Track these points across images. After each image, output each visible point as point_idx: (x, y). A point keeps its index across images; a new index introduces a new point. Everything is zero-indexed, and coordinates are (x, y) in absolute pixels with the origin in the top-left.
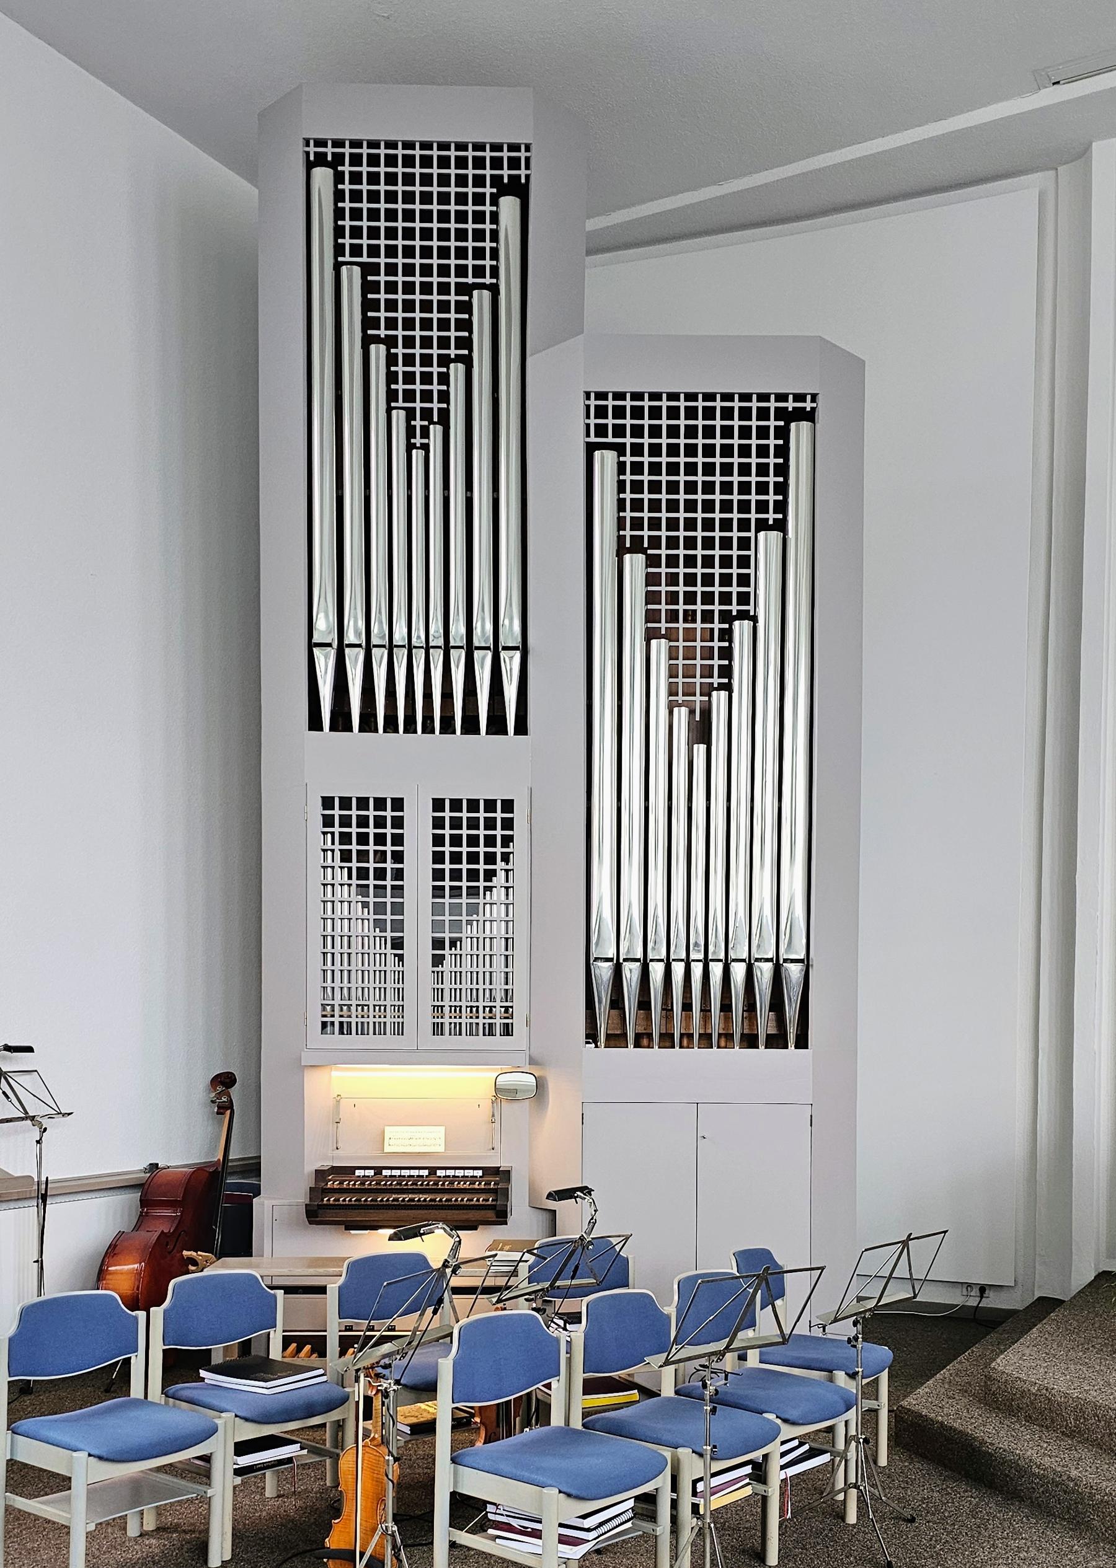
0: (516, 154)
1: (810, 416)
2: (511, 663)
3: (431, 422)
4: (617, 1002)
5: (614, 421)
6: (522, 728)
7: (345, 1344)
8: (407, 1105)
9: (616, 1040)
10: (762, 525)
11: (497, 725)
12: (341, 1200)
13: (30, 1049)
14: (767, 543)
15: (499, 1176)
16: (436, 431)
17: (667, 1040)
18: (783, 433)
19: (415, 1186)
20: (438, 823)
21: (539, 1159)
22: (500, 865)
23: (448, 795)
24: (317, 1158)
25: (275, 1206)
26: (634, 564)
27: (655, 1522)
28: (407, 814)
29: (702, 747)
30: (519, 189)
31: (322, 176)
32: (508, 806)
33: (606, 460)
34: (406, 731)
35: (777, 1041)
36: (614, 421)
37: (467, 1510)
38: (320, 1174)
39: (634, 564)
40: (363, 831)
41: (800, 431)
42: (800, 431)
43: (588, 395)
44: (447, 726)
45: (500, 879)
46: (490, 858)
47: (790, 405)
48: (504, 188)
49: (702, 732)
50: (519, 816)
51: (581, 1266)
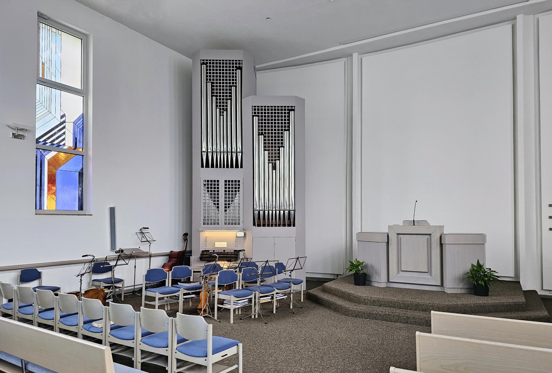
1: (294, 110)
5: (257, 111)
6: (242, 167)
8: (219, 239)
9: (259, 225)
10: (285, 130)
12: (206, 256)
16: (225, 112)
18: (289, 113)
20: (226, 185)
23: (227, 179)
24: (202, 248)
25: (194, 258)
26: (262, 137)
28: (220, 183)
30: (240, 68)
32: (239, 181)
33: (256, 119)
35: (289, 225)
36: (257, 111)
37: (221, 302)
39: (262, 137)
40: (212, 186)
41: (292, 113)
42: (292, 113)
44: (227, 167)
46: (236, 191)
47: (290, 108)
48: (238, 68)
49: (274, 168)
50: (241, 183)
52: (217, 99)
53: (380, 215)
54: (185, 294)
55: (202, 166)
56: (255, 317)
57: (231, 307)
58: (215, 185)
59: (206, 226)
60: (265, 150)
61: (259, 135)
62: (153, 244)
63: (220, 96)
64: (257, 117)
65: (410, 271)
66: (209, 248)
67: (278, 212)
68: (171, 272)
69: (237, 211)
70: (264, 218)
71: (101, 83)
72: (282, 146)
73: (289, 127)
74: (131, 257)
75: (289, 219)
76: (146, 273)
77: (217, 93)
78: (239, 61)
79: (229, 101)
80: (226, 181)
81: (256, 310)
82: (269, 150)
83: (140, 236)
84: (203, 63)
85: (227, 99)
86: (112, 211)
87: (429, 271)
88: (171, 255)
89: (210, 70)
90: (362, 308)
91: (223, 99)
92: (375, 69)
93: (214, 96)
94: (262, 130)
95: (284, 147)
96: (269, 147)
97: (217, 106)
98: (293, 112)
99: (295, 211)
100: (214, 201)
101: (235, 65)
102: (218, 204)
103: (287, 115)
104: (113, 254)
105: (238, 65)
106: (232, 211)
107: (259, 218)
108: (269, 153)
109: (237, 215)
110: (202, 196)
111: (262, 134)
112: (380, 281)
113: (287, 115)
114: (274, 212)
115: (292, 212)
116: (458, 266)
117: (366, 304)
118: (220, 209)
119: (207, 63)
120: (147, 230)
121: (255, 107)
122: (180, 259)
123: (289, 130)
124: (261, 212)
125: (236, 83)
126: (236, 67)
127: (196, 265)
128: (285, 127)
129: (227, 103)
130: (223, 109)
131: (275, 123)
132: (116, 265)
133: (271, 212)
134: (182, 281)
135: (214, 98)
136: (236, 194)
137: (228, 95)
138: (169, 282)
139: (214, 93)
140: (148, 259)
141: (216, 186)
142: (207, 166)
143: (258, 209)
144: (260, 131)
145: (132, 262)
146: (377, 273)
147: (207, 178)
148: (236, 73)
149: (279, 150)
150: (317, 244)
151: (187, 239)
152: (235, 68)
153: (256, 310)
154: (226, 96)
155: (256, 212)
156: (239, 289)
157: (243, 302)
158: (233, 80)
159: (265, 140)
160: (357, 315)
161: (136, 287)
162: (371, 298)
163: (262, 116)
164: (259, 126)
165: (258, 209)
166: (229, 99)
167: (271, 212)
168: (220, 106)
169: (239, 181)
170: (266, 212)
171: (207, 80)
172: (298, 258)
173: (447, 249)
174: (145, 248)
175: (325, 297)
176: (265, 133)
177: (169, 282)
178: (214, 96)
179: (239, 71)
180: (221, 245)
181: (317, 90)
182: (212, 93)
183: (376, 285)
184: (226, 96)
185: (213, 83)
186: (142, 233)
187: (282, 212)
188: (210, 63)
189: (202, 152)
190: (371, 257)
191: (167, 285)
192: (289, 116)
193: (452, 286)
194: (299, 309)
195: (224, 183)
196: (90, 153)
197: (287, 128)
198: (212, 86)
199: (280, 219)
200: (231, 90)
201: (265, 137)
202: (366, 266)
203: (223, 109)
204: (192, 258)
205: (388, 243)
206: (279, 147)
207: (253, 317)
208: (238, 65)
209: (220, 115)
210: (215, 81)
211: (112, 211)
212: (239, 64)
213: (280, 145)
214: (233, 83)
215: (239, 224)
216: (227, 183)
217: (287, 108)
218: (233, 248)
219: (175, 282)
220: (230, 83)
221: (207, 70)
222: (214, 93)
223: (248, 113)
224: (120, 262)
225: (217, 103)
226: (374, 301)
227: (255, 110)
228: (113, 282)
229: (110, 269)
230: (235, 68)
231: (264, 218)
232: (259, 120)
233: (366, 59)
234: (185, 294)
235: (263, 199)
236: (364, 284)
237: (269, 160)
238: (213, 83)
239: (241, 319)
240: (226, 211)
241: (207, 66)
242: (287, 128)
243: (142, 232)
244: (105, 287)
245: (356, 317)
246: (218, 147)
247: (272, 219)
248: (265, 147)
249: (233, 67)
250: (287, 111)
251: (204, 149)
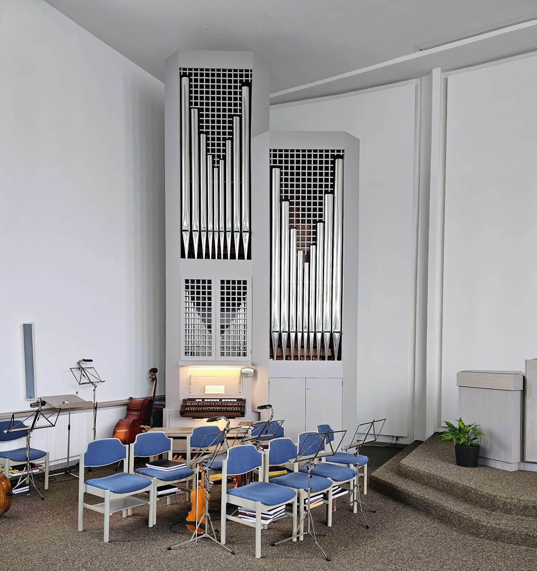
0: (248, 73)
1: (342, 157)
2: (246, 236)
3: (220, 159)
5: (278, 158)
6: (249, 257)
8: (211, 378)
9: (280, 357)
10: (327, 192)
11: (241, 256)
12: (191, 409)
13: (91, 361)
14: (328, 198)
15: (242, 402)
16: (222, 162)
17: (288, 358)
18: (333, 162)
19: (215, 405)
20: (222, 288)
21: (255, 396)
22: (242, 301)
23: (226, 279)
24: (184, 396)
25: (170, 411)
26: (286, 204)
28: (213, 285)
29: (307, 263)
30: (248, 84)
31: (185, 80)
33: (276, 172)
34: (212, 258)
35: (331, 358)
36: (278, 158)
37: (232, 509)
38: (185, 401)
39: (286, 204)
40: (198, 290)
41: (339, 162)
42: (339, 162)
43: (270, 150)
45: (242, 306)
46: (239, 299)
47: (336, 153)
48: (243, 84)
49: (307, 259)
50: (248, 285)
51: (268, 430)
52: (208, 139)
54: (159, 489)
55: (183, 256)
56: (298, 538)
58: (204, 288)
59: (190, 357)
60: (291, 227)
61: (281, 200)
62: (99, 386)
63: (213, 133)
64: (278, 170)
66: (195, 394)
67: (312, 335)
68: (132, 445)
69: (242, 333)
70: (289, 346)
72: (320, 221)
73: (333, 186)
74: (58, 411)
75: (331, 346)
76: (85, 450)
77: (207, 127)
78: (247, 71)
79: (228, 143)
80: (222, 282)
81: (298, 529)
82: (297, 228)
83: (77, 373)
84: (185, 75)
85: (224, 139)
86: (28, 329)
88: (130, 406)
89: (196, 92)
91: (219, 139)
92: (471, 96)
93: (203, 132)
94: (286, 192)
95: (324, 222)
96: (298, 221)
97: (208, 150)
98: (340, 160)
99: (341, 333)
100: (204, 315)
101: (238, 79)
102: (210, 321)
103: (330, 165)
105: (244, 79)
106: (231, 334)
107: (280, 346)
108: (298, 234)
109: (242, 340)
110: (180, 306)
111: (286, 199)
112: (506, 460)
113: (330, 165)
114: (306, 335)
115: (337, 335)
117: (508, 511)
118: (213, 329)
119: (190, 74)
120: (89, 364)
121: (275, 150)
122: (145, 413)
123: (332, 192)
124: (284, 336)
125: (241, 111)
126: (241, 81)
127: (173, 424)
128: (327, 186)
129: (224, 145)
130: (219, 156)
131: (310, 180)
132: (33, 428)
133: (300, 335)
134: (151, 460)
135: (203, 136)
136: (239, 305)
137: (227, 131)
138: (129, 464)
139: (202, 127)
140: (91, 413)
141: (207, 290)
142: (191, 255)
143: (278, 330)
144: (283, 195)
145: (63, 418)
146: (502, 446)
147: (194, 275)
148: (241, 93)
149: (315, 227)
151: (156, 379)
152: (239, 84)
153: (298, 529)
154: (224, 133)
155: (276, 335)
156: (264, 483)
158: (235, 105)
159: (291, 210)
161: (70, 460)
162: (519, 500)
163: (286, 168)
164: (281, 186)
165: (278, 330)
166: (229, 139)
167: (300, 335)
168: (213, 151)
169: (245, 282)
170: (293, 335)
171: (191, 104)
172: (372, 423)
174: (86, 395)
175: (403, 485)
176: (292, 197)
177: (129, 464)
178: (203, 132)
179: (245, 89)
181: (375, 130)
182: (200, 127)
183: (499, 466)
184: (224, 133)
185: (202, 110)
186: (80, 368)
187: (319, 335)
188: (196, 75)
189: (182, 231)
191: (125, 470)
192: (333, 168)
195: (219, 285)
197: (329, 189)
198: (200, 116)
199: (315, 347)
200: (231, 122)
201: (291, 204)
202: (461, 431)
203: (218, 157)
204: (166, 411)
205: (524, 392)
206: (315, 222)
207: (295, 540)
208: (244, 79)
209: (213, 167)
210: (205, 107)
211: (28, 329)
212: (247, 76)
213: (318, 219)
214: (236, 111)
215: (245, 355)
216: (225, 285)
217: (330, 153)
218: (234, 394)
219: (140, 462)
220: (230, 110)
221: (191, 86)
222: (202, 127)
223: (262, 162)
224: (42, 421)
225: (208, 145)
226: (526, 507)
227: (275, 156)
228: (27, 459)
229: (25, 433)
230: (239, 84)
231: (289, 346)
232: (281, 174)
233: (454, 78)
234: (159, 489)
235: (285, 315)
236: (475, 464)
237: (298, 246)
238: (202, 110)
239: (273, 545)
240: (222, 332)
241: (191, 80)
242: (329, 189)
243: (82, 366)
244: (14, 468)
245: (496, 539)
246: (211, 223)
247: (302, 347)
248: (291, 221)
249: (236, 82)
250: (330, 159)
251: (186, 224)
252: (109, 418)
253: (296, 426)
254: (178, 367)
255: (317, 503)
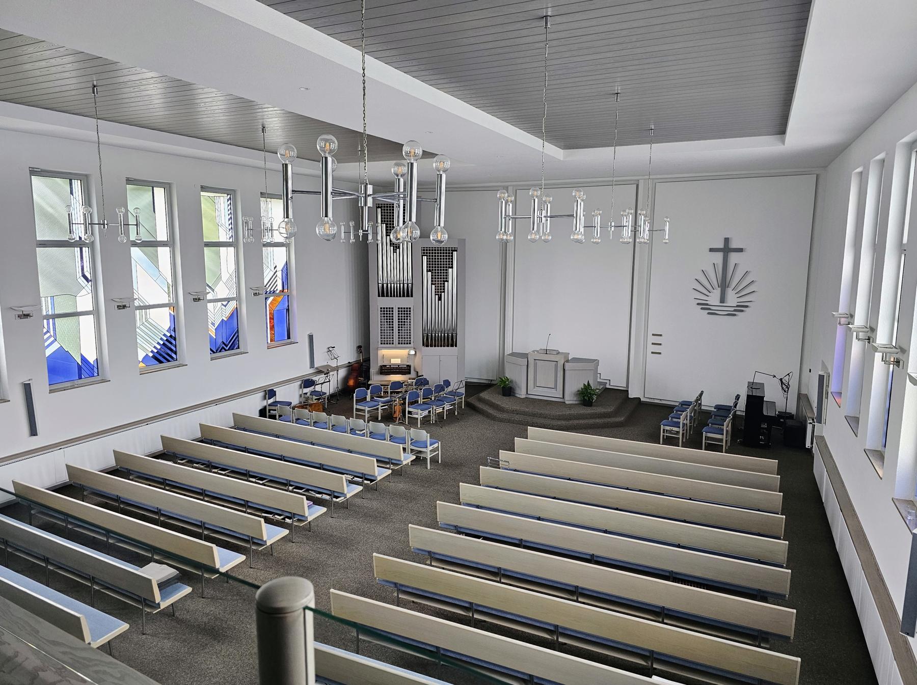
4: (427, 339)
7: (391, 393)
8: (395, 355)
9: (427, 346)
11: (408, 296)
12: (386, 370)
15: (409, 366)
19: (396, 368)
21: (416, 364)
24: (380, 363)
25: (373, 370)
26: (430, 273)
27: (426, 251)
31: (379, 210)
35: (452, 346)
36: (426, 251)
37: (410, 413)
38: (381, 367)
39: (430, 273)
40: (387, 313)
41: (455, 253)
42: (455, 253)
49: (440, 299)
51: (422, 382)
53: (526, 337)
57: (419, 417)
65: (539, 386)
71: (299, 237)
81: (433, 418)
86: (311, 338)
87: (555, 388)
90: (505, 416)
104: (312, 371)
112: (521, 393)
116: (574, 385)
142: (383, 296)
150: (476, 354)
153: (433, 418)
157: (426, 413)
160: (501, 420)
173: (567, 372)
174: (333, 364)
180: (396, 361)
190: (514, 374)
193: (570, 399)
194: (462, 414)
196: (294, 293)
202: (512, 382)
211: (311, 338)
252: (342, 373)
253: (434, 377)
254: (377, 349)
255: (440, 410)
